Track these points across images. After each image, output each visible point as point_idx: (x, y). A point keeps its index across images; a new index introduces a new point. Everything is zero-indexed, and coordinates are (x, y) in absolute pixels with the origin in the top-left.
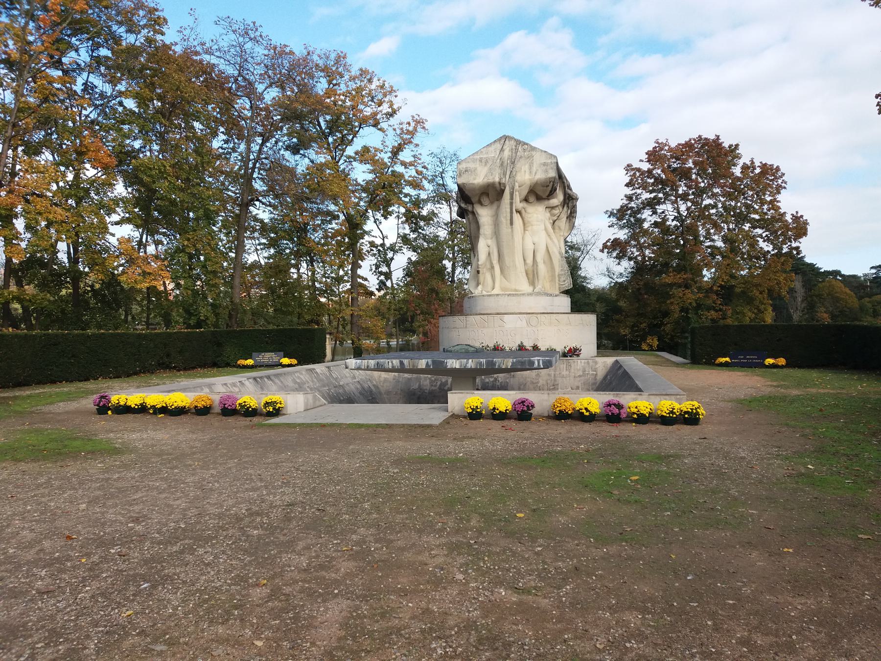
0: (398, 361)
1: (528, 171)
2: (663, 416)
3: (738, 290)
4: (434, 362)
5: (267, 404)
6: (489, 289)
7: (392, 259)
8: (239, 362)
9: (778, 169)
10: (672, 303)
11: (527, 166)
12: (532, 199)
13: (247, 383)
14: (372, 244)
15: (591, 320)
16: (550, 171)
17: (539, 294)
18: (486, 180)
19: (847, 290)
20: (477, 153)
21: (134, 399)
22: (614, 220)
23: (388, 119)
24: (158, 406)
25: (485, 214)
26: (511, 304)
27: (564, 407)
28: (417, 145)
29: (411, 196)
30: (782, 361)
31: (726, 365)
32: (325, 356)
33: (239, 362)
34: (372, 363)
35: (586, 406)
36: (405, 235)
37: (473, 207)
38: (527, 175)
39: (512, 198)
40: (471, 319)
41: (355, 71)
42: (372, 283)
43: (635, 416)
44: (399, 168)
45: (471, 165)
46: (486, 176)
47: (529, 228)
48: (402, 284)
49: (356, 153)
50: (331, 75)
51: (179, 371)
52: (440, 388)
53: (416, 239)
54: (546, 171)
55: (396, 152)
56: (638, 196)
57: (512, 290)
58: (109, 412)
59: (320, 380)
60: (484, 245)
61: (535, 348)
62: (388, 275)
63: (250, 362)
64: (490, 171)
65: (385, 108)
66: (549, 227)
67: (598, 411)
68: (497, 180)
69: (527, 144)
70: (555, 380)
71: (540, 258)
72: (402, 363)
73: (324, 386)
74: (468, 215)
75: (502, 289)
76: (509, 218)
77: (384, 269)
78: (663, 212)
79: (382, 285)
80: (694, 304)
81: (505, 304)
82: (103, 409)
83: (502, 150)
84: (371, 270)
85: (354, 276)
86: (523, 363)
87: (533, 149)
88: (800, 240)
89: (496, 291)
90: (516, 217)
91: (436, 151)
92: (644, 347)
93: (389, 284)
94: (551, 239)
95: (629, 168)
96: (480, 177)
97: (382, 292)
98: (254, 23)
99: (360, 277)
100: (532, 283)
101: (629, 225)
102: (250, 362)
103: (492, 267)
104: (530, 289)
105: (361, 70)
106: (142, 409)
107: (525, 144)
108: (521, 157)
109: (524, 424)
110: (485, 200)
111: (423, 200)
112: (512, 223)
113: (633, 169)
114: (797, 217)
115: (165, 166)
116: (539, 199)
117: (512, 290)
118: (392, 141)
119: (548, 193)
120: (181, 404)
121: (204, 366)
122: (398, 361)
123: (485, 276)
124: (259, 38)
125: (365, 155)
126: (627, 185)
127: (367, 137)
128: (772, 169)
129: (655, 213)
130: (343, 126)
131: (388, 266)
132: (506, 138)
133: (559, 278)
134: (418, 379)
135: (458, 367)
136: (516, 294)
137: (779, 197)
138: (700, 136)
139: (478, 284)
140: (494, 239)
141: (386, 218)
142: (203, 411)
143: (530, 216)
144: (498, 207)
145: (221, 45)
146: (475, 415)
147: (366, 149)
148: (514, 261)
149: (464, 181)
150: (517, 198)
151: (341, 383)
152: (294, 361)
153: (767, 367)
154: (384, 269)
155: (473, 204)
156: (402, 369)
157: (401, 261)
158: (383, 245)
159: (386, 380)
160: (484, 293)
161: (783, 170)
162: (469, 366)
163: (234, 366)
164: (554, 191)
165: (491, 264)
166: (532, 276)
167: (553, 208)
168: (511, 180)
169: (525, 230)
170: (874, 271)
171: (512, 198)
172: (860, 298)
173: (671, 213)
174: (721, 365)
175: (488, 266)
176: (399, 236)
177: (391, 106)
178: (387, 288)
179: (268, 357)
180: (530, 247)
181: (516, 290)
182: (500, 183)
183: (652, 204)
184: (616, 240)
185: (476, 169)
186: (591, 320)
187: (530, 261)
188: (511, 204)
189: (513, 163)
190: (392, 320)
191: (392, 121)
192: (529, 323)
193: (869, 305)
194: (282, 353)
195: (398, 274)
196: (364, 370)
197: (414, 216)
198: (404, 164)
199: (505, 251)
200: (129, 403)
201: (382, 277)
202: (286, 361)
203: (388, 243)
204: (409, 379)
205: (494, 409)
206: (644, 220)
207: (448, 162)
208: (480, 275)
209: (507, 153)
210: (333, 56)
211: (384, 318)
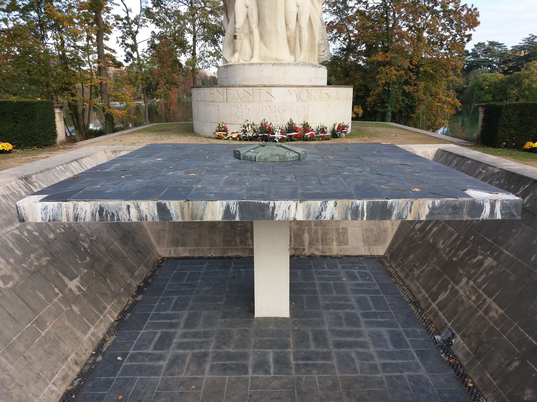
4: (242, 207)
6: (247, 57)
7: (137, 32)
10: (380, 79)
14: (117, 18)
15: (346, 94)
17: (304, 64)
22: (327, 7)
32: (55, 135)
36: (148, 9)
40: (233, 91)
42: (120, 56)
48: (146, 55)
53: (158, 13)
62: (134, 48)
72: (163, 210)
75: (261, 58)
77: (130, 41)
79: (129, 56)
81: (268, 74)
84: (118, 42)
85: (100, 46)
88: (475, 28)
89: (255, 60)
93: (135, 55)
97: (130, 63)
99: (107, 48)
100: (293, 52)
103: (251, 32)
104: (291, 59)
123: (243, 43)
131: (134, 38)
133: (319, 47)
136: (277, 63)
139: (234, 51)
154: (130, 41)
157: (146, 33)
158: (127, 18)
160: (242, 62)
162: (327, 215)
165: (250, 28)
175: (247, 30)
176: (142, 10)
178: (134, 59)
181: (276, 59)
186: (346, 94)
187: (293, 25)
190: (141, 87)
192: (299, 98)
195: (143, 46)
199: (267, 13)
201: (129, 49)
203: (132, 16)
208: (238, 41)
211: (135, 86)
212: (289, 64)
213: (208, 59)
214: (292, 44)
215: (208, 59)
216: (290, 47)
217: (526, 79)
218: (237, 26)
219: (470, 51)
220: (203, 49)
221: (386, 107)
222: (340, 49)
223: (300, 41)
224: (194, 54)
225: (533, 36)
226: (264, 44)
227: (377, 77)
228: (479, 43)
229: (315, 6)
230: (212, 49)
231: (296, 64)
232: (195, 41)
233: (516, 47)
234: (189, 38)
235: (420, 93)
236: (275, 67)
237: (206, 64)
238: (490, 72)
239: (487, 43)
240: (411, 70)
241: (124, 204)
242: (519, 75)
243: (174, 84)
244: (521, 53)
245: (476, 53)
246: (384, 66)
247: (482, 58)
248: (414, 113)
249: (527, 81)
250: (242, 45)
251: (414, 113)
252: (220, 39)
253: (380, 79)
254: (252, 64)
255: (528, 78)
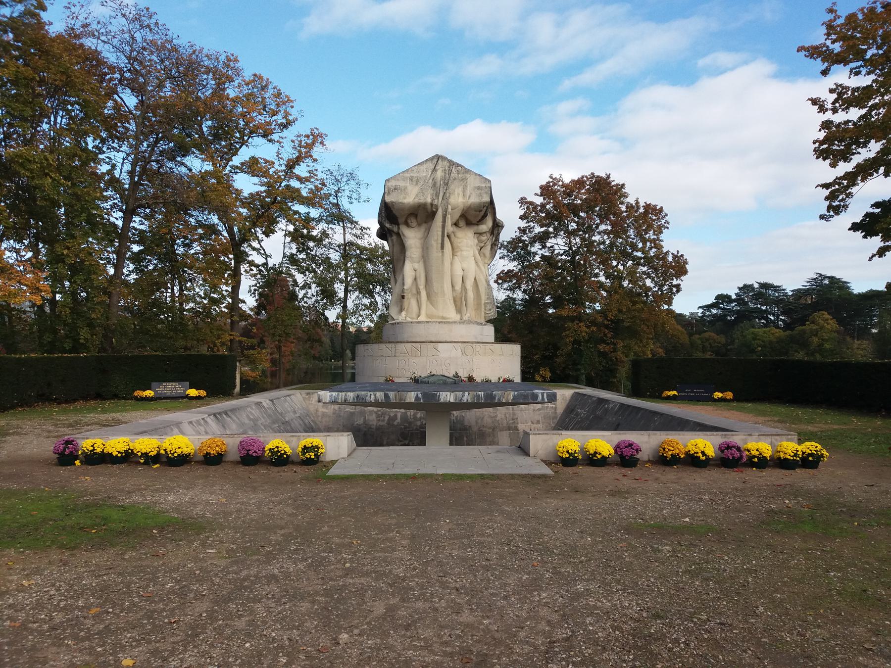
0: (382, 393)
1: (461, 193)
2: (786, 459)
3: (626, 324)
4: (424, 395)
5: (306, 449)
6: (414, 315)
8: (136, 394)
9: (661, 209)
10: (567, 336)
11: (460, 189)
12: (462, 223)
13: (209, 420)
16: (485, 195)
17: (469, 322)
18: (417, 200)
19: (679, 327)
20: (407, 170)
21: (116, 444)
23: (282, 130)
24: (152, 454)
25: (412, 237)
26: (443, 332)
27: (677, 451)
28: (315, 160)
29: (300, 214)
30: (729, 395)
31: (674, 398)
33: (136, 394)
34: (351, 395)
35: (702, 449)
36: (292, 255)
37: (399, 228)
38: (460, 198)
39: (444, 221)
40: (401, 347)
41: (248, 75)
43: (756, 460)
44: (295, 184)
45: (401, 184)
46: (417, 195)
47: (459, 254)
49: (242, 164)
50: (222, 79)
51: (59, 403)
52: (388, 424)
54: (481, 195)
55: (292, 165)
56: (531, 229)
57: (438, 317)
58: (77, 463)
59: (269, 416)
60: (411, 269)
61: (471, 379)
63: (149, 393)
64: (422, 191)
65: (279, 118)
66: (477, 252)
67: (714, 455)
68: (429, 200)
69: (461, 166)
70: (514, 414)
71: (469, 284)
72: (386, 396)
73: (274, 423)
74: (391, 236)
75: (428, 316)
76: (440, 242)
78: (552, 247)
80: (587, 338)
82: (66, 456)
83: (434, 170)
84: (250, 291)
86: (525, 397)
87: (467, 171)
89: (422, 318)
90: (446, 239)
91: (332, 168)
92: (538, 378)
94: (478, 266)
95: (523, 201)
96: (410, 197)
98: (148, 9)
100: (459, 310)
101: (518, 258)
102: (149, 393)
103: (418, 293)
104: (457, 317)
105: (255, 75)
106: (128, 457)
107: (459, 165)
108: (455, 179)
109: (628, 471)
110: (412, 221)
111: (313, 219)
112: (442, 247)
113: (526, 203)
114: (676, 256)
115: (47, 160)
116: (469, 223)
117: (438, 317)
118: (289, 153)
119: (480, 218)
120: (186, 451)
121: (86, 398)
122: (382, 393)
124: (153, 26)
125: (252, 167)
126: (522, 218)
127: (257, 148)
128: (656, 209)
129: (544, 247)
130: (226, 136)
132: (438, 158)
133: (485, 307)
134: (362, 413)
135: (452, 400)
137: (662, 237)
138: (592, 174)
139: (401, 310)
140: (421, 264)
141: (267, 236)
142: (212, 460)
143: (459, 240)
144: (428, 230)
145: (110, 28)
146: (569, 461)
147: (254, 161)
148: (442, 287)
149: (393, 200)
150: (449, 222)
151: (287, 419)
152: (203, 393)
153: (715, 400)
155: (398, 225)
156: (334, 402)
159: (324, 415)
160: (409, 319)
161: (665, 210)
163: (131, 399)
164: (480, 216)
166: (459, 303)
167: (481, 234)
168: (444, 202)
169: (453, 255)
170: (701, 311)
171: (444, 221)
172: (691, 335)
173: (562, 248)
174: (669, 398)
175: (414, 291)
176: (284, 256)
177: (285, 117)
179: (171, 388)
180: (459, 273)
181: (443, 318)
182: (432, 205)
183: (542, 238)
184: (509, 271)
185: (406, 188)
187: (458, 287)
188: (443, 227)
189: (447, 184)
191: (285, 133)
192: (464, 353)
193: (699, 342)
194: (188, 383)
196: (341, 404)
197: (302, 236)
198: (299, 179)
199: (434, 276)
200: (108, 450)
202: (193, 392)
204: (352, 414)
205: (596, 453)
206: (535, 254)
207: (345, 179)
209: (439, 174)
210: (222, 58)
212: (455, 322)
213: (362, 313)
214: (459, 304)
215: (362, 313)
216: (456, 306)
217: (814, 338)
218: (405, 287)
219: (734, 297)
220: (357, 302)
221: (579, 370)
222: (522, 300)
223: (466, 301)
224: (345, 307)
225: (821, 275)
226: (432, 304)
227: (564, 334)
228: (745, 285)
229: (480, 269)
230: (367, 301)
231: (462, 322)
232: (346, 291)
233: (799, 290)
234: (339, 288)
235: (619, 353)
236: (441, 325)
237: (360, 319)
238: (765, 326)
239: (756, 286)
240: (607, 327)
241: (369, 393)
242: (804, 331)
243: (317, 341)
244: (806, 300)
245: (743, 300)
246: (573, 321)
247: (751, 306)
248: (615, 377)
249: (815, 340)
250: (409, 304)
251: (615, 377)
252: (377, 290)
253: (567, 336)
254: (419, 322)
255: (816, 335)
